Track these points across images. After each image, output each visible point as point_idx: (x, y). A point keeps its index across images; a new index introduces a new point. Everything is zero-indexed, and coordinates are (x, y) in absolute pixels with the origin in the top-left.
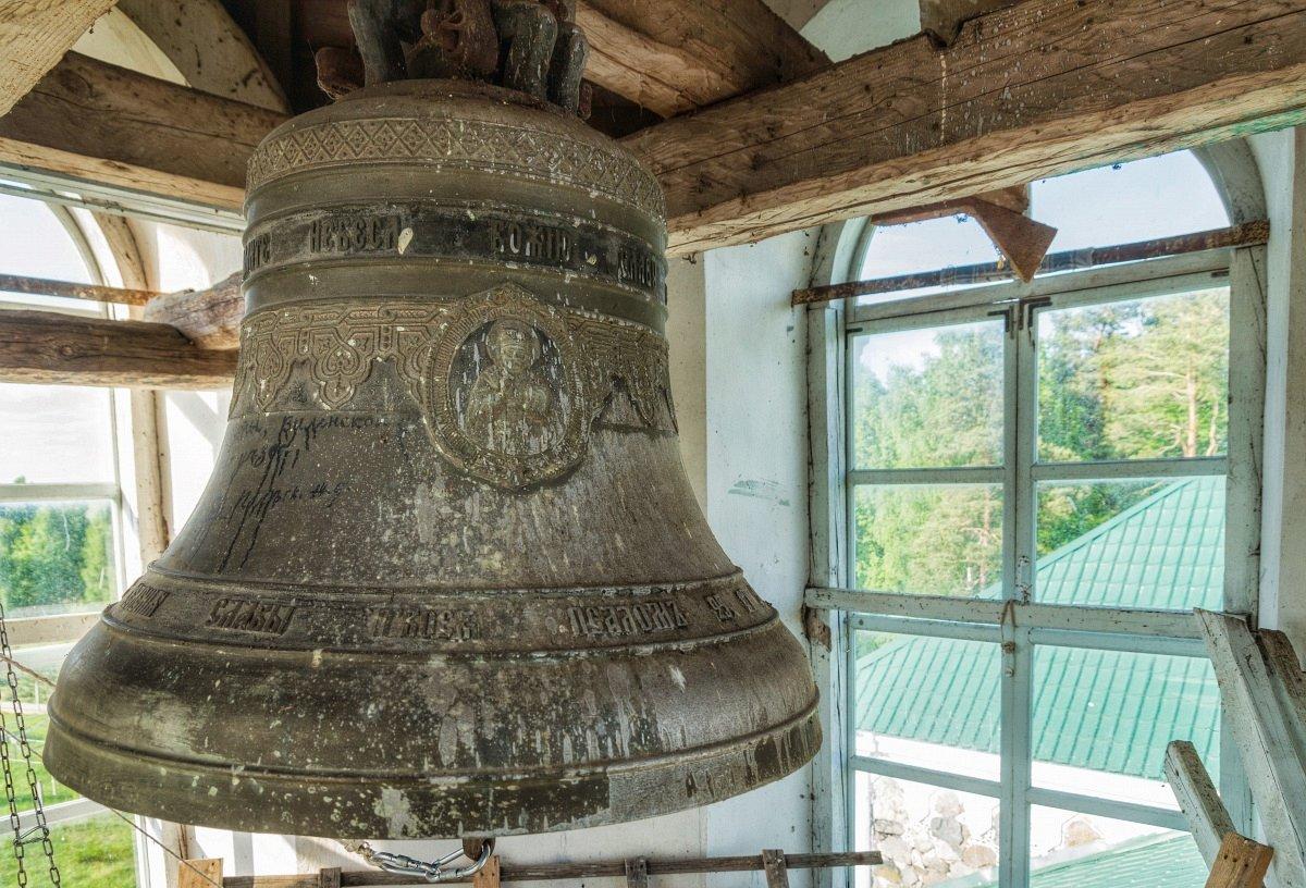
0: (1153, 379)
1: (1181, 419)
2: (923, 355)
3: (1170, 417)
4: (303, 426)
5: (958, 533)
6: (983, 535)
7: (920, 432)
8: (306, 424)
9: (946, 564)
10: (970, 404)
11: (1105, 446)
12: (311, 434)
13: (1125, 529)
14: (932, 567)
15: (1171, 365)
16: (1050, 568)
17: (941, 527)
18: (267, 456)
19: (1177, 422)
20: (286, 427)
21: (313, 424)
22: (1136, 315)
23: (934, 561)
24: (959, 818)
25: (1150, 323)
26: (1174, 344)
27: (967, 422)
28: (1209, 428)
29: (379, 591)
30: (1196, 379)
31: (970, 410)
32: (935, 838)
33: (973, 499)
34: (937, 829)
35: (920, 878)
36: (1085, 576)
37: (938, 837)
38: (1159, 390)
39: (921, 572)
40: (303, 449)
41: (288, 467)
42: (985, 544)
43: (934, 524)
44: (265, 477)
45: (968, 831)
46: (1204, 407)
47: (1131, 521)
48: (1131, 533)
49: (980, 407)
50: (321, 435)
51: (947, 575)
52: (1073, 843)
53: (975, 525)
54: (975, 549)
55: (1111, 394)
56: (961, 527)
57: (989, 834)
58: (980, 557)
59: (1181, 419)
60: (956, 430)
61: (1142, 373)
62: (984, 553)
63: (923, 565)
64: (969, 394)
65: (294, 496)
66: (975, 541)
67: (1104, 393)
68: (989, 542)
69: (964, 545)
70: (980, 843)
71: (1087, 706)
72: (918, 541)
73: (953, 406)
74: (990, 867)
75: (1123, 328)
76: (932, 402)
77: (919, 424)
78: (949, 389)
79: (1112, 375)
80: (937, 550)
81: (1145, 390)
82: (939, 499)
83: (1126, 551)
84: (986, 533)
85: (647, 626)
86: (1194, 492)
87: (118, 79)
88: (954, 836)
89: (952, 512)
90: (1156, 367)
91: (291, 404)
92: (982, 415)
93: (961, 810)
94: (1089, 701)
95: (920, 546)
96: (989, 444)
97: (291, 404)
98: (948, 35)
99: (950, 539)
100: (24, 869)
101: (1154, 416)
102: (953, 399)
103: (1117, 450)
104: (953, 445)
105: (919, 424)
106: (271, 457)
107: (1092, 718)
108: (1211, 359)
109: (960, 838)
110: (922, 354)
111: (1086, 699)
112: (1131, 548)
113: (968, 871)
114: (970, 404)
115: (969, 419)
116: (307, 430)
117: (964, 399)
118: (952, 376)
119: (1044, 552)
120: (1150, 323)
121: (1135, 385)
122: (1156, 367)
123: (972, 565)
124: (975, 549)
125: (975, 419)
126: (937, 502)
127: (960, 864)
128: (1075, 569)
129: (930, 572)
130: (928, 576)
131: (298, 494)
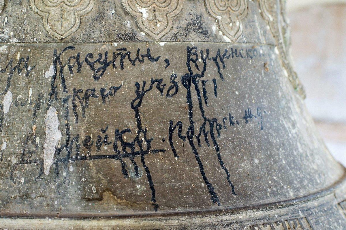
4: (210, 56)
8: (212, 55)
12: (220, 64)
18: (180, 85)
20: (193, 57)
21: (218, 54)
29: (245, 213)
40: (218, 78)
41: (211, 95)
44: (191, 106)
50: (228, 62)
65: (232, 123)
85: (137, 174)
91: (193, 35)
97: (193, 35)
98: (276, 36)
100: (133, 111)
106: (188, 87)
116: (215, 60)
131: (234, 120)
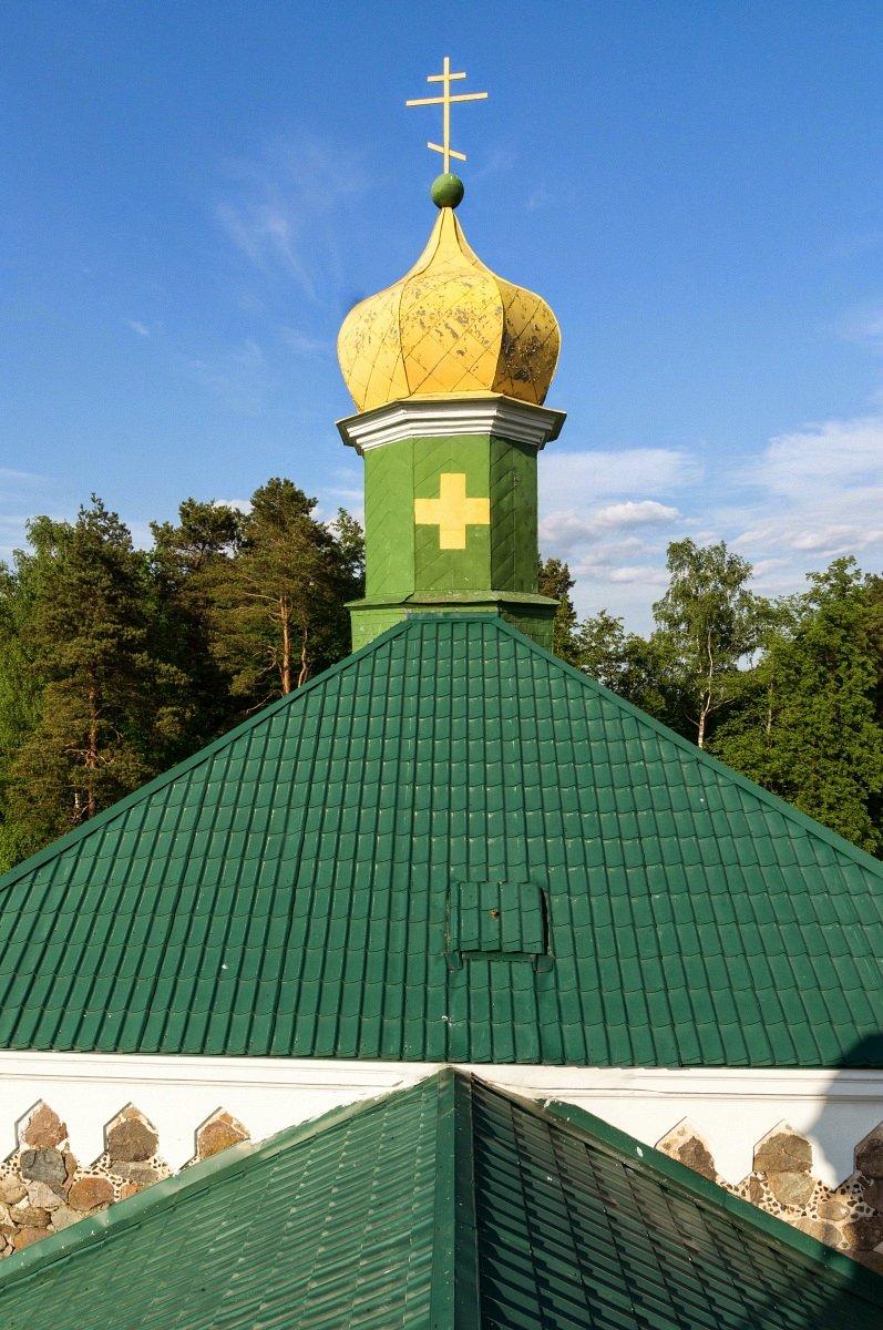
0: (250, 602)
1: (276, 642)
2: (15, 552)
3: (266, 640)
5: (62, 756)
6: (90, 757)
7: (15, 641)
9: (48, 790)
10: (71, 611)
11: (210, 666)
13: (250, 740)
14: (34, 793)
15: (266, 587)
16: (166, 791)
17: (43, 749)
19: (273, 645)
22: (232, 538)
23: (36, 787)
24: (60, 1147)
25: (245, 545)
26: (269, 567)
27: (67, 632)
28: (300, 651)
30: (288, 602)
31: (72, 619)
32: (28, 1181)
33: (76, 717)
34: (30, 1167)
35: (9, 1240)
36: (208, 801)
37: (32, 1179)
38: (255, 611)
39: (21, 801)
42: (92, 766)
43: (35, 746)
45: (74, 1162)
46: (295, 632)
47: (111, 826)
48: (258, 743)
49: (82, 615)
51: (51, 802)
52: (210, 1153)
53: (79, 746)
54: (82, 773)
55: (214, 612)
56: (66, 748)
57: (102, 1161)
58: (87, 782)
59: (276, 642)
60: (56, 640)
61: (240, 594)
62: (91, 777)
63: (24, 792)
64: (69, 600)
66: (82, 762)
67: (207, 611)
68: (97, 765)
69: (69, 767)
70: (91, 1176)
71: (220, 968)
72: (15, 765)
73: (51, 613)
74: (106, 1206)
75: (221, 549)
76: (28, 607)
77: (14, 631)
78: (46, 593)
79: (214, 593)
80: (38, 774)
81: (242, 612)
82: (40, 718)
83: (253, 766)
84: (92, 754)
86: (321, 697)
87: (730, 1186)
88: (55, 1172)
89: (55, 731)
90: (254, 590)
92: (84, 625)
93: (64, 1134)
94: (221, 963)
95: (18, 770)
96: (93, 656)
99: (53, 762)
101: (253, 637)
102: (51, 604)
103: (221, 669)
104: (53, 656)
105: (14, 631)
107: (227, 986)
108: (301, 584)
109: (61, 1174)
110: (15, 552)
111: (218, 961)
112: (241, 762)
113: (76, 1218)
114: (71, 611)
115: (71, 628)
117: (65, 605)
118: (50, 579)
119: (154, 774)
120: (245, 545)
121: (235, 606)
122: (254, 590)
123: (79, 791)
124: (82, 773)
125: (76, 628)
126: (38, 721)
127: (64, 1210)
128: (196, 789)
129: (31, 800)
130: (30, 805)
